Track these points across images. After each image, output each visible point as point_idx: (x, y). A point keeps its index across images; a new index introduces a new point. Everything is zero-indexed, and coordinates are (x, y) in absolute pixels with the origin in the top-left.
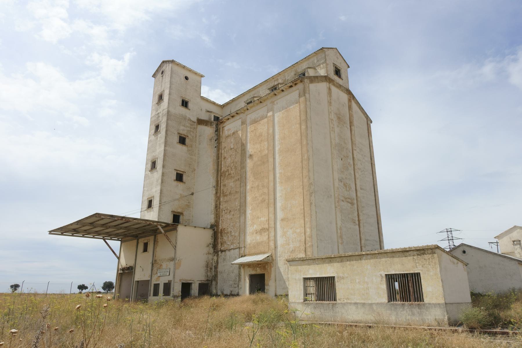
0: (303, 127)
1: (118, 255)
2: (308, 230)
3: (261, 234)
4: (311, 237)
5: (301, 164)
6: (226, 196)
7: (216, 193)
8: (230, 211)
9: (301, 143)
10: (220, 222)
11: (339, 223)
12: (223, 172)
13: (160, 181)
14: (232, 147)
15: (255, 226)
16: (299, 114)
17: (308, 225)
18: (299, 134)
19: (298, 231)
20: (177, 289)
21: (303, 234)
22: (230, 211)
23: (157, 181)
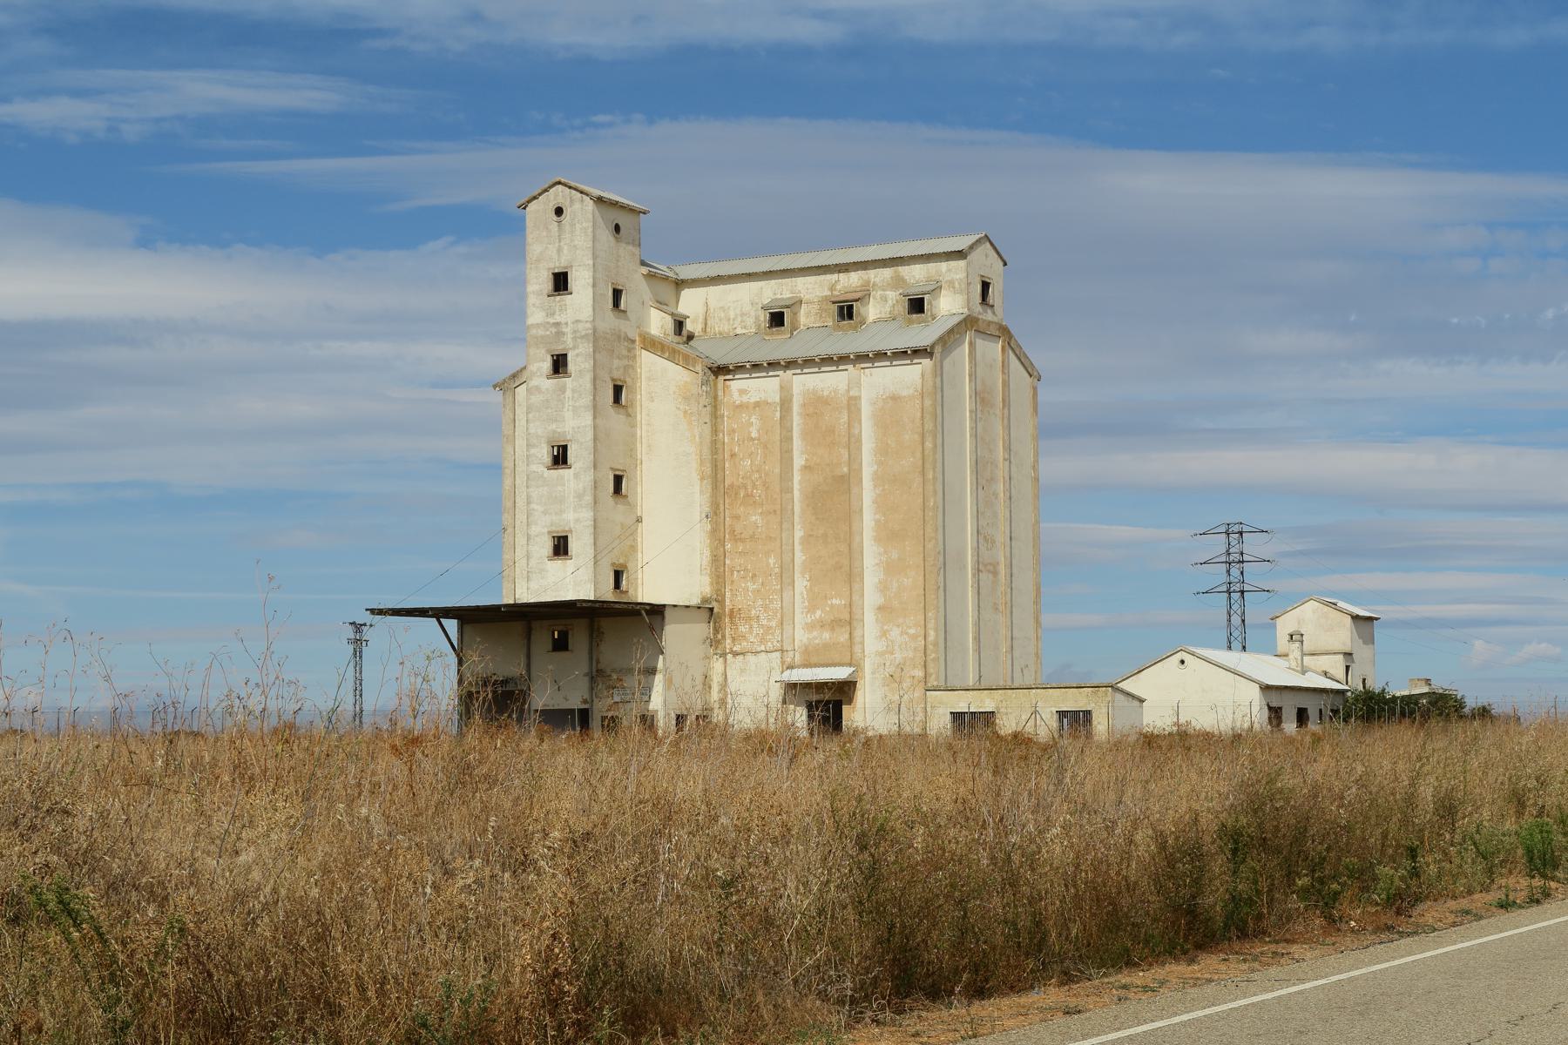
0: (929, 445)
1: (1124, 685)
2: (932, 634)
3: (833, 629)
4: (936, 644)
5: (920, 513)
6: (742, 540)
7: (714, 531)
8: (754, 576)
9: (923, 474)
10: (728, 595)
11: (509, 449)
12: (732, 486)
13: (589, 498)
14: (754, 435)
15: (818, 613)
16: (919, 414)
17: (931, 625)
18: (919, 455)
19: (912, 631)
20: (595, 723)
21: (921, 638)
22: (754, 576)
23: (580, 496)
